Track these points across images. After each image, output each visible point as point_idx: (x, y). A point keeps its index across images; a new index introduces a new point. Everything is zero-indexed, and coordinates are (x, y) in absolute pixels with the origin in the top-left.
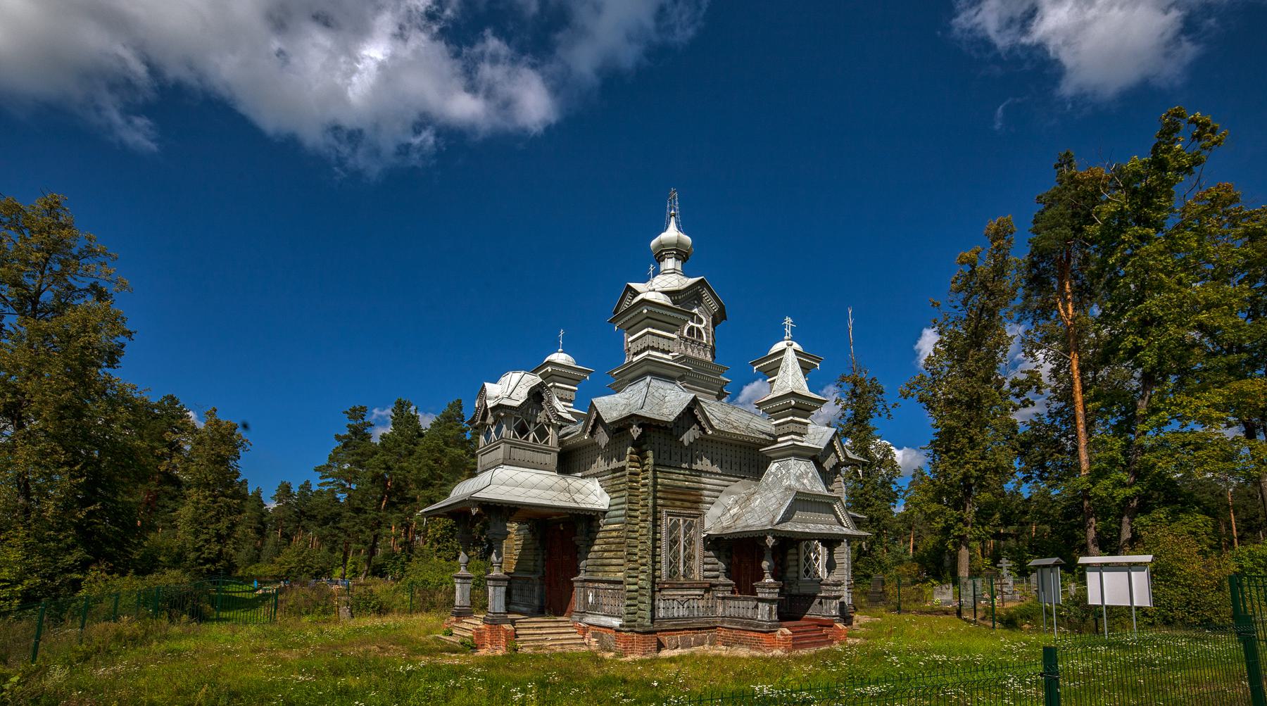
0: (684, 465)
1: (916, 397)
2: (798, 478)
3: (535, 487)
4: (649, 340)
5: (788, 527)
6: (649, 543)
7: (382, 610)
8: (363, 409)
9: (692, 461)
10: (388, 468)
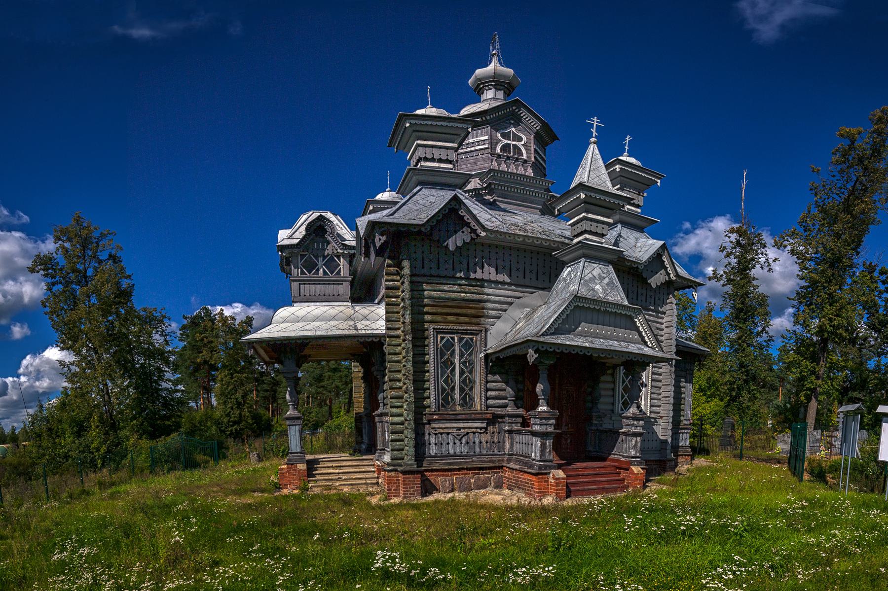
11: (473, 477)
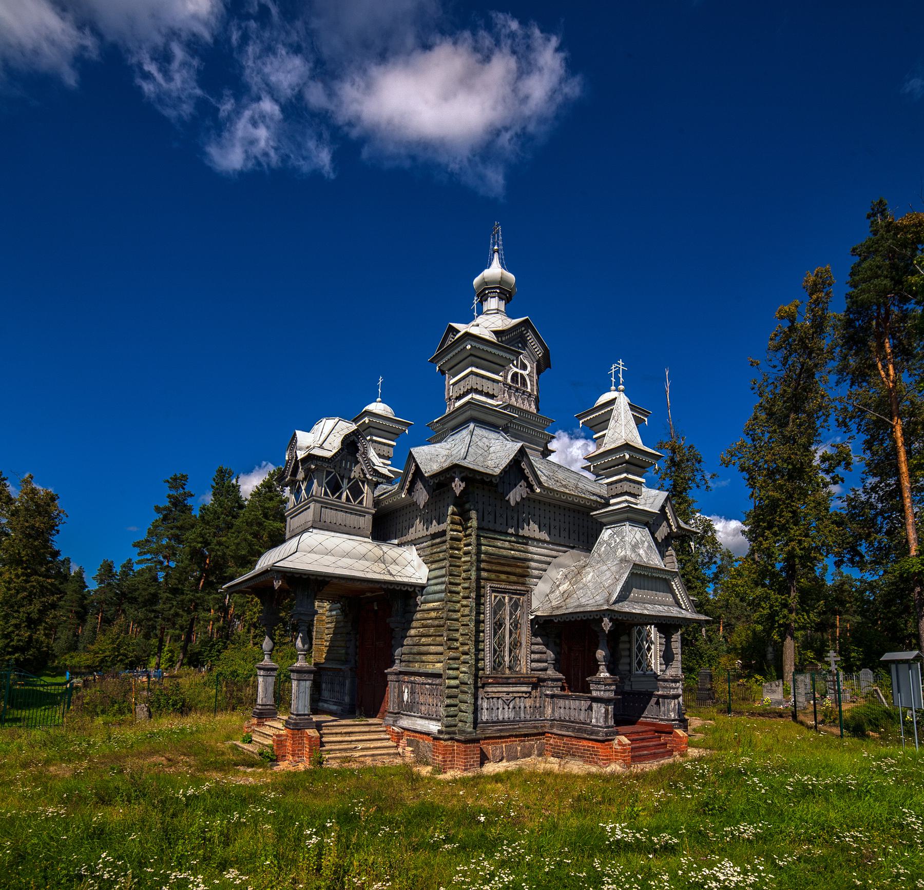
0: (511, 531)
1: (737, 467)
2: (635, 547)
3: (347, 555)
4: (473, 382)
5: (626, 607)
6: (472, 625)
7: (184, 708)
8: (185, 478)
9: (518, 526)
10: (206, 543)
11: (519, 745)
